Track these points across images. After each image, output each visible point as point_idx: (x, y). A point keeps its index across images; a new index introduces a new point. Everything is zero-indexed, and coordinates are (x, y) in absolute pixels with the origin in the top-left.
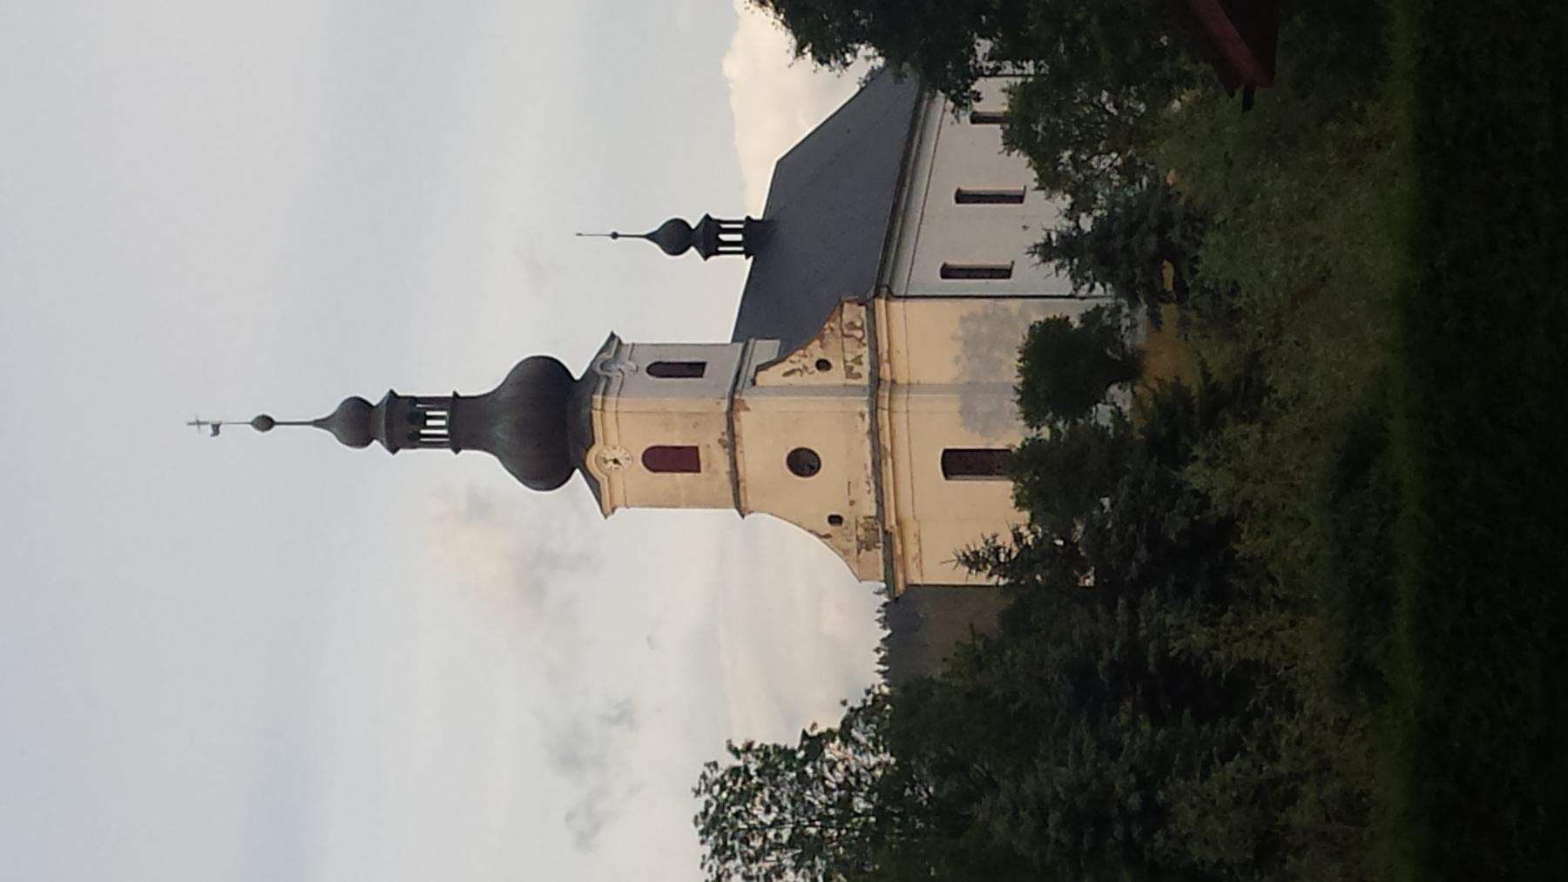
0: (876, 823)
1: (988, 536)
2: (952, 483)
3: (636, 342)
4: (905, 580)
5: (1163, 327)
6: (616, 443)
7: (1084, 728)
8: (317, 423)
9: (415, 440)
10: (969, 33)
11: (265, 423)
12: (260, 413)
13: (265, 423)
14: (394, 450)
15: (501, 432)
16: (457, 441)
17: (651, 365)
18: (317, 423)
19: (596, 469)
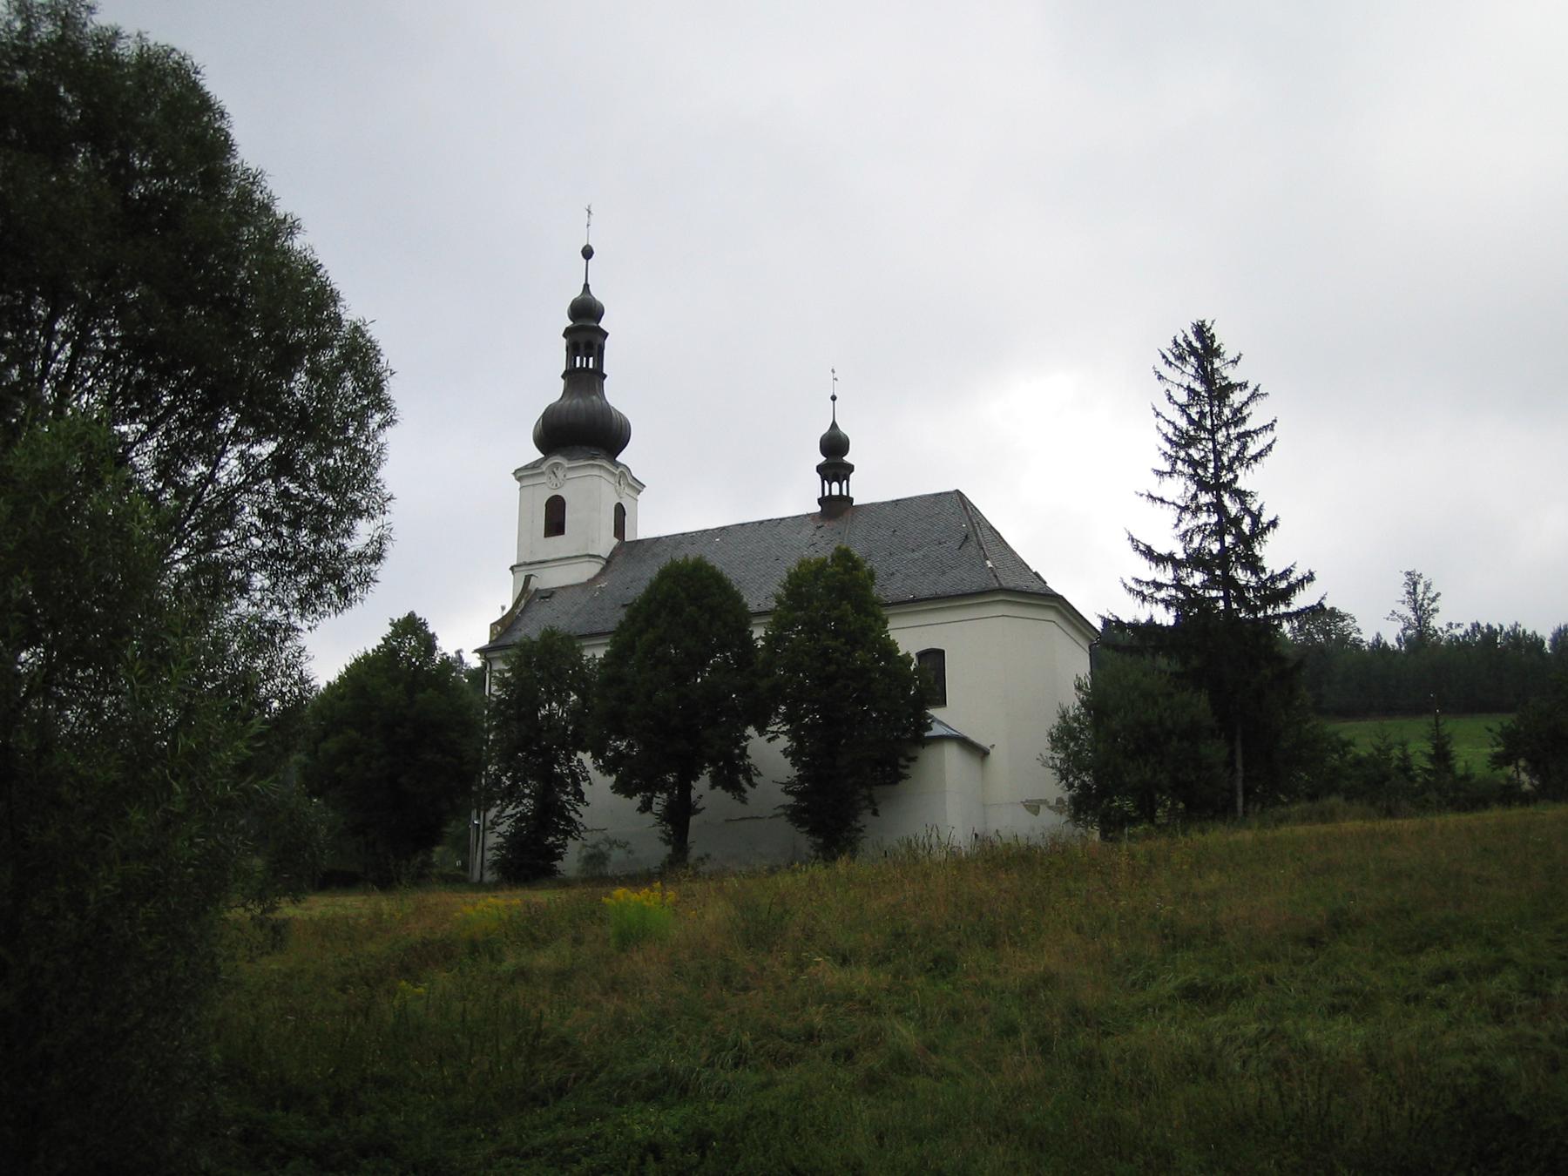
0: (11, 421)
1: (381, 352)
2: (608, 331)
3: (639, 503)
4: (493, 658)
5: (746, 795)
6: (567, 477)
7: (1292, 810)
8: (586, 286)
9: (573, 350)
10: (565, 715)
11: (588, 253)
12: (594, 249)
13: (588, 253)
14: (563, 377)
15: (577, 402)
16: (571, 375)
17: (622, 505)
18: (586, 286)
19: (551, 462)
